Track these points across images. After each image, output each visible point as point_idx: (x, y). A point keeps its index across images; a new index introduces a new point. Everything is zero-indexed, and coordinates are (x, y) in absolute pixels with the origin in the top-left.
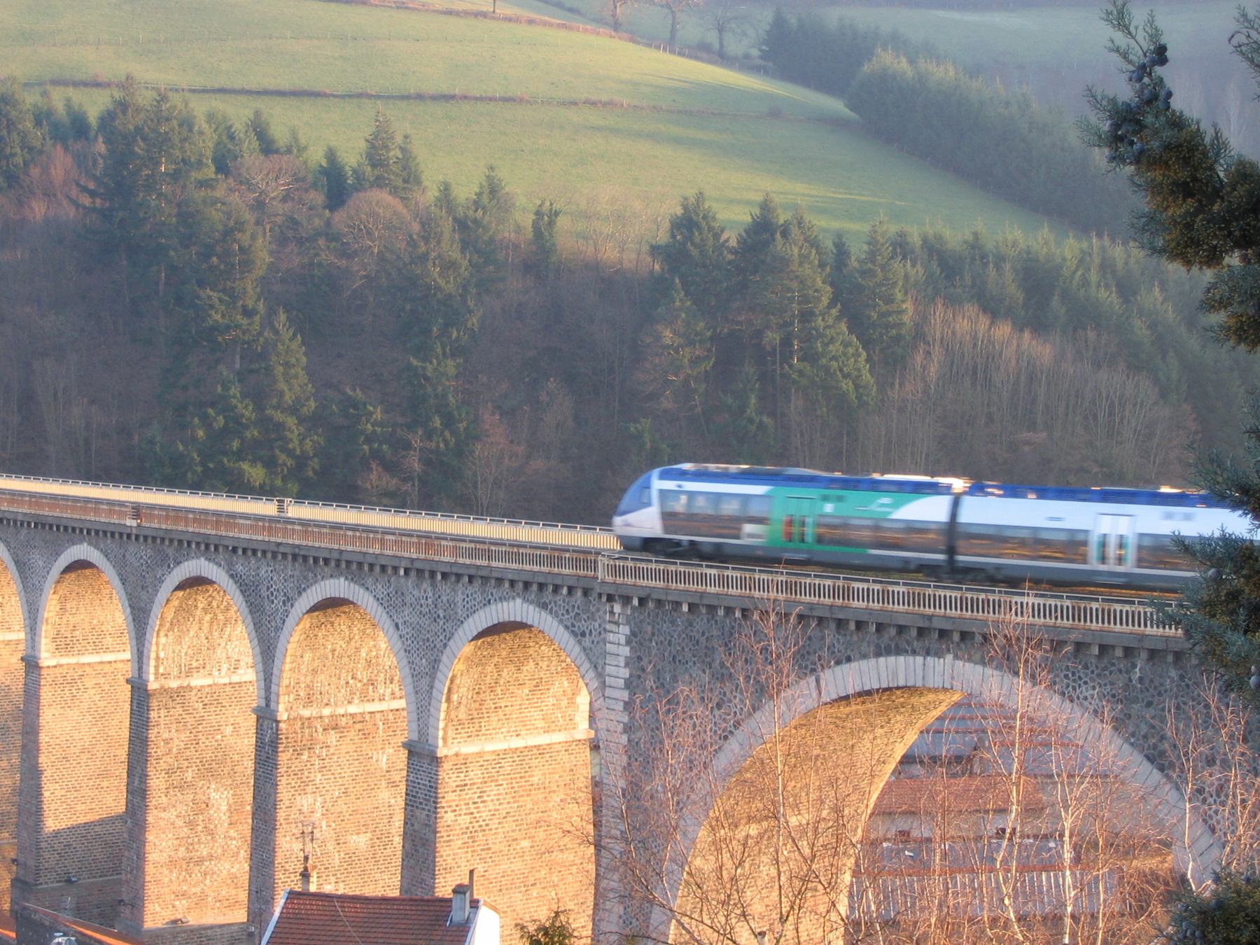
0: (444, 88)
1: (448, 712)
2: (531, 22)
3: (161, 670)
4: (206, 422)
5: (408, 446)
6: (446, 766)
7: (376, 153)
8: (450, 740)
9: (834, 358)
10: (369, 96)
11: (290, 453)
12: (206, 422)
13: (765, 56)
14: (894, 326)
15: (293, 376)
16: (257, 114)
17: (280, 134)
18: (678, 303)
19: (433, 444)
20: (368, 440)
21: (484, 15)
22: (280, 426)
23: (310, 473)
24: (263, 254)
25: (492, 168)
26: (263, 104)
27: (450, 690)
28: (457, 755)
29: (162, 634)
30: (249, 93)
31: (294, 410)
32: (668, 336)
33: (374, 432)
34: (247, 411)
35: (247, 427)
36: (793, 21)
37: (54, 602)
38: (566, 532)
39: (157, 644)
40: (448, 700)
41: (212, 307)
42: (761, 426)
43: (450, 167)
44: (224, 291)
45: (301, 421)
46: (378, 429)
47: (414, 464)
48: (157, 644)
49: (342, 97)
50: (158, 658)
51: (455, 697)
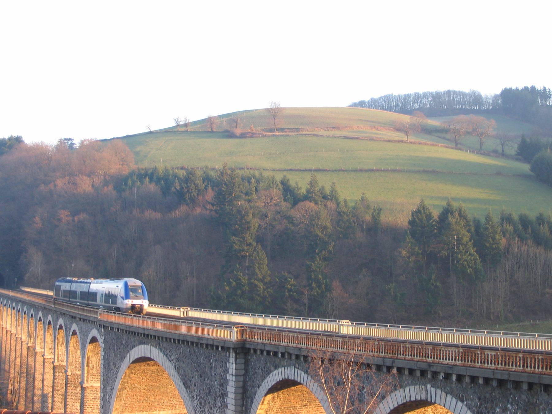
0: (371, 167)
1: (88, 371)
2: (420, 143)
3: (60, 358)
4: (229, 284)
5: (302, 293)
6: (88, 390)
7: (333, 190)
8: (90, 381)
9: (465, 260)
10: (343, 171)
11: (259, 295)
12: (229, 284)
13: (519, 154)
14: (496, 248)
15: (263, 267)
16: (285, 176)
17: (292, 183)
18: (408, 240)
19: (312, 293)
20: (290, 290)
21: (402, 141)
22: (256, 286)
23: (267, 303)
24: (255, 222)
25: (364, 194)
26: (285, 173)
27: (88, 362)
28: (92, 386)
29: (59, 345)
30: (300, 170)
31: (262, 281)
32: (404, 253)
33: (291, 288)
34: (245, 280)
35: (243, 286)
36: (528, 140)
37: (49, 336)
38: (446, 333)
39: (58, 349)
40: (88, 366)
41: (235, 243)
42: (436, 287)
43: (349, 193)
44: (242, 238)
45: (265, 284)
46: (293, 288)
47: (305, 300)
48: (58, 349)
49: (333, 171)
50: (58, 354)
51: (91, 365)
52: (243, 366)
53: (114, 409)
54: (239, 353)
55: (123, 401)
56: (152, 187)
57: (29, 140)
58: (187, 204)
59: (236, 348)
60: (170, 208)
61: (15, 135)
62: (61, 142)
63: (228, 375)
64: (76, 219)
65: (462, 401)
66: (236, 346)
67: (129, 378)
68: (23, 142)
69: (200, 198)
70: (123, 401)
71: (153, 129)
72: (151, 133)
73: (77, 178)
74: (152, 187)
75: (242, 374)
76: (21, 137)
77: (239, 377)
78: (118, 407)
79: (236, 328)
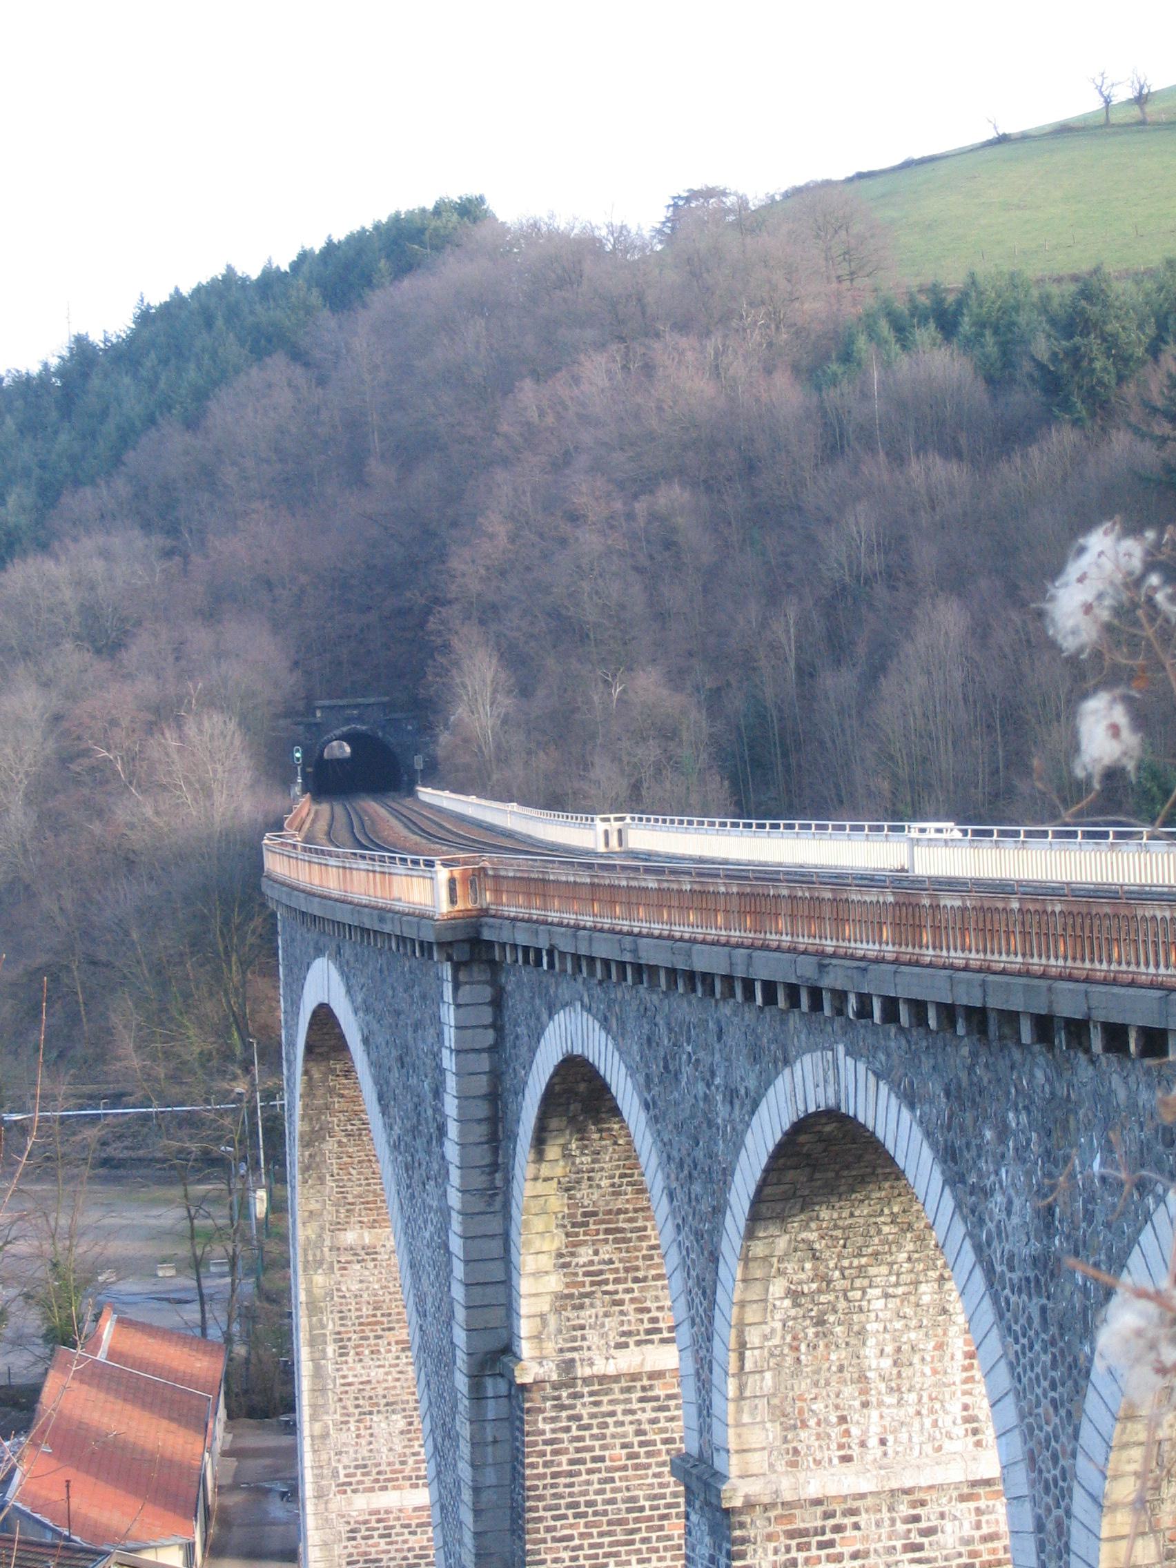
52: (487, 1015)
53: (300, 1215)
54: (466, 964)
55: (330, 1183)
56: (941, 364)
57: (509, 209)
58: (1076, 423)
59: (450, 944)
60: (1012, 436)
61: (455, 194)
62: (680, 208)
63: (444, 1050)
64: (640, 507)
65: (912, 1107)
66: (449, 937)
67: (331, 1091)
68: (494, 218)
69: (1130, 389)
70: (330, 1183)
71: (1012, 127)
72: (1003, 139)
73: (657, 345)
74: (941, 364)
75: (486, 1045)
76: (481, 200)
77: (472, 1056)
78: (314, 1206)
79: (445, 864)
